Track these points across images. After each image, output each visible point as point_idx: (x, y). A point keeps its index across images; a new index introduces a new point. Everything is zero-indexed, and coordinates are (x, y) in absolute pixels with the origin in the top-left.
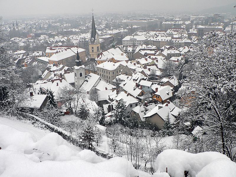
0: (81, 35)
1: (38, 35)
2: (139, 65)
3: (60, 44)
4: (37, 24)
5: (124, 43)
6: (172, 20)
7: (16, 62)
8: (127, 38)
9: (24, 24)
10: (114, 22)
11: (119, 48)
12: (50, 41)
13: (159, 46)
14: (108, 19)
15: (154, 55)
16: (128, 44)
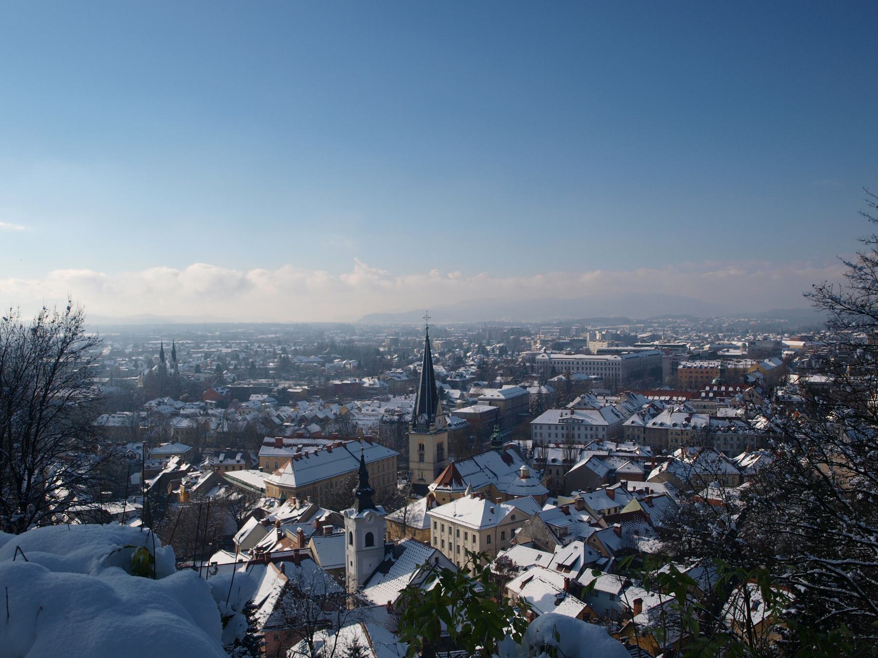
0: (388, 400)
3: (315, 428)
5: (538, 435)
6: (712, 355)
7: (151, 482)
8: (551, 417)
9: (200, 355)
14: (489, 348)
15: (643, 477)
16: (553, 436)
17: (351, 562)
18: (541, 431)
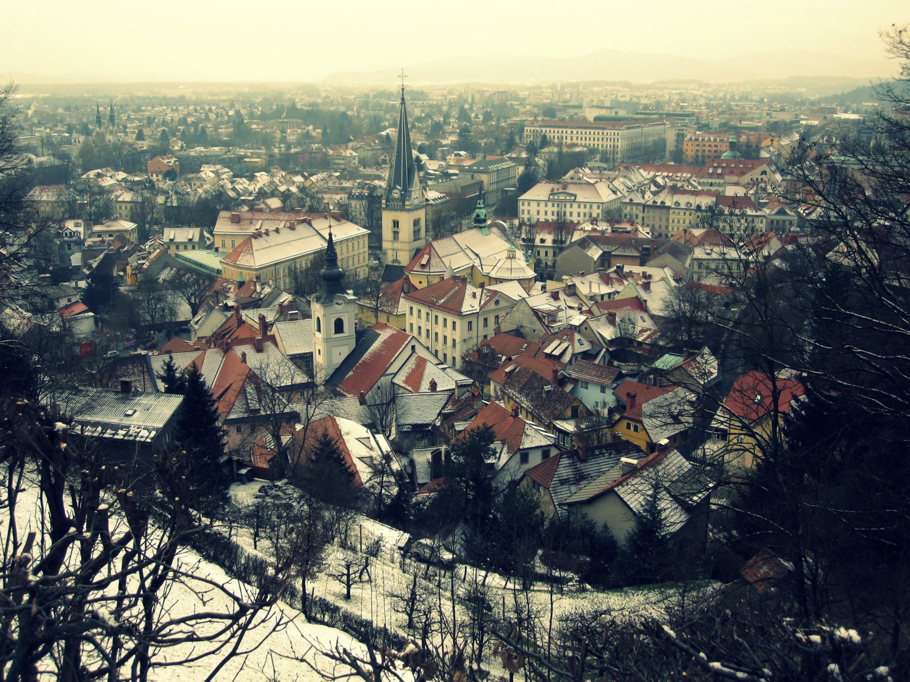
1: (190, 167)
2: (572, 302)
4: (190, 120)
5: (526, 212)
10: (498, 127)
11: (503, 230)
12: (234, 189)
13: (663, 228)
17: (319, 350)
18: (529, 208)
